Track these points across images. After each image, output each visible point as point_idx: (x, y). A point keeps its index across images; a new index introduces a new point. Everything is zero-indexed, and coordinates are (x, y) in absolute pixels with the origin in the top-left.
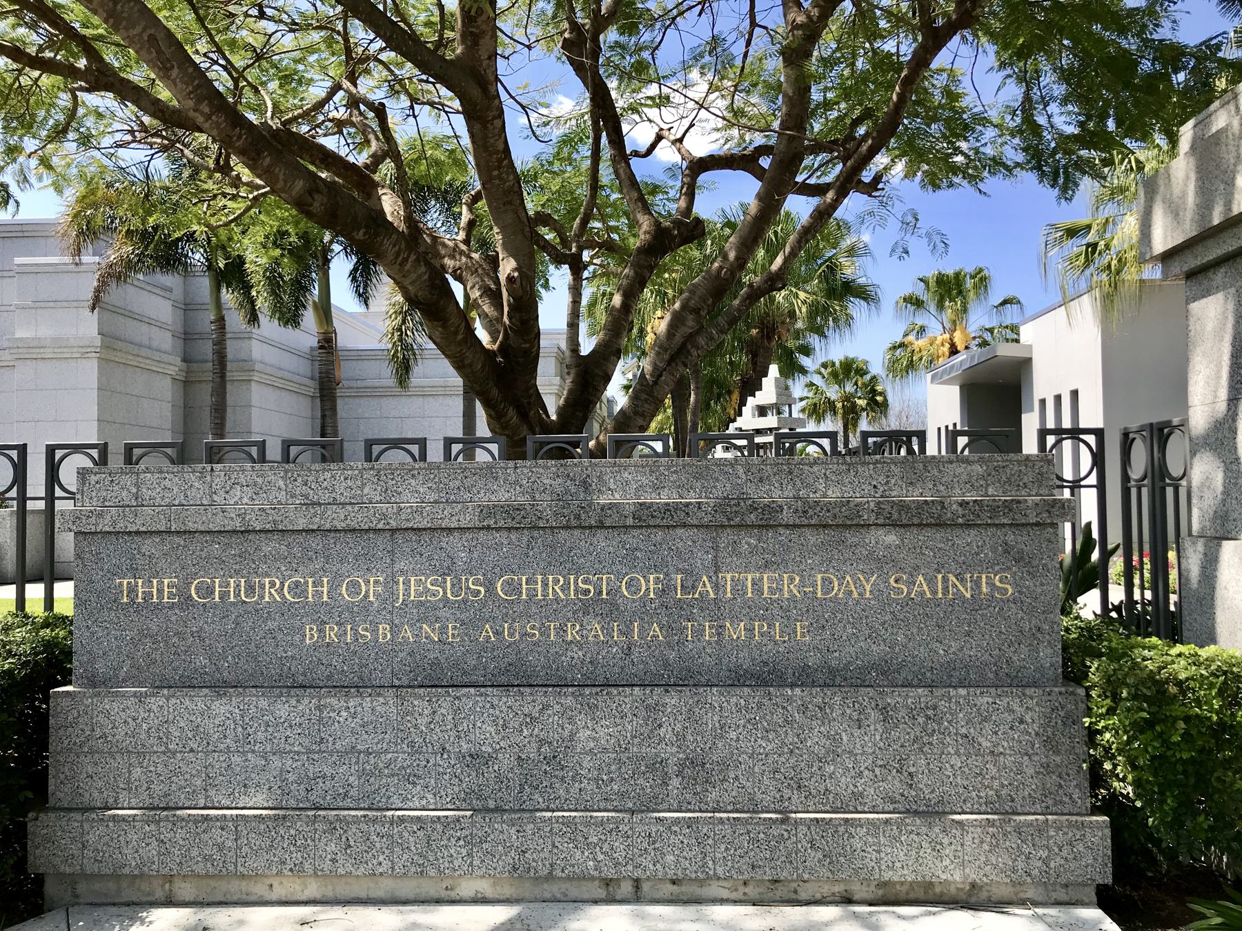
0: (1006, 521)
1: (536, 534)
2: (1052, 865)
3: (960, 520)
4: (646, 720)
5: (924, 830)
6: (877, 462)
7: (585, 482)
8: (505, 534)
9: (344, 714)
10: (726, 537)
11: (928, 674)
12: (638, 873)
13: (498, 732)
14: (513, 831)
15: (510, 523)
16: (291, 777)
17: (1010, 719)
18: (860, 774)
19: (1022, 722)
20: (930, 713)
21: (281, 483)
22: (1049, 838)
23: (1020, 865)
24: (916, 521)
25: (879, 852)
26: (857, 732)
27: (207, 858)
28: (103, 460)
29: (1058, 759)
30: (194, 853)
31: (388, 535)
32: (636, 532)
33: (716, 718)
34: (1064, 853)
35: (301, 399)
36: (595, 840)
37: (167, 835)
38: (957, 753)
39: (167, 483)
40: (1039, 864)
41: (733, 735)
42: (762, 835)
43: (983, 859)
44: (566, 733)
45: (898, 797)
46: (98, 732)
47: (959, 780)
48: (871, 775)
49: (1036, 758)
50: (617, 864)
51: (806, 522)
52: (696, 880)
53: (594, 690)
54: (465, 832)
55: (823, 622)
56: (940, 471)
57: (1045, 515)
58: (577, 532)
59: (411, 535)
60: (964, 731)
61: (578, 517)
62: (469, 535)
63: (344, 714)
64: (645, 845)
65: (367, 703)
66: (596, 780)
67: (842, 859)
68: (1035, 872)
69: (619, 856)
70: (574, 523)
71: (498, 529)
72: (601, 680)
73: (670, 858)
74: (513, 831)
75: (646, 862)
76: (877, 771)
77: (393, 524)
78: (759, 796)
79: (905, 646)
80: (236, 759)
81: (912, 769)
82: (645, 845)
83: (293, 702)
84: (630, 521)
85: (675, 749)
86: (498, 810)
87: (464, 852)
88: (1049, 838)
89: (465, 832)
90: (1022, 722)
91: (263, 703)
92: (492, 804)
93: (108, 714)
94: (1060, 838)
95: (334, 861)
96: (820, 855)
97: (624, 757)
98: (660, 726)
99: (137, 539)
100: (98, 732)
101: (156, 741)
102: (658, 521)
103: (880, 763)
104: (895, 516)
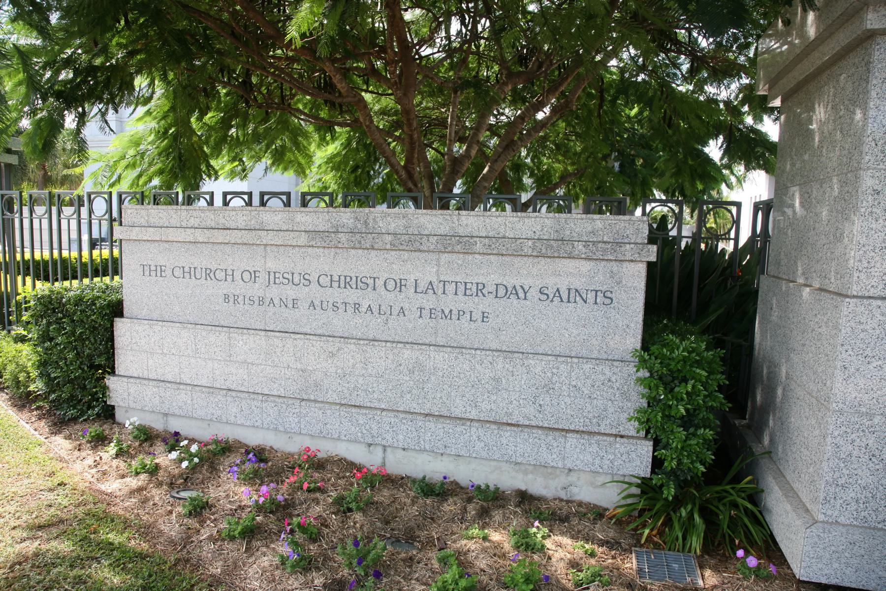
0: (612, 258)
1: (338, 251)
2: (616, 463)
3: (583, 256)
4: (393, 361)
5: (543, 437)
6: (537, 217)
7: (366, 222)
8: (321, 250)
9: (241, 342)
10: (445, 258)
11: (558, 348)
12: (384, 442)
13: (315, 360)
14: (320, 412)
15: (325, 245)
16: (217, 372)
17: (602, 378)
18: (511, 402)
19: (609, 381)
20: (554, 371)
21: (212, 217)
22: (616, 448)
23: (597, 461)
24: (556, 255)
25: (516, 446)
26: (511, 379)
27: (180, 408)
28: (249, 203)
29: (629, 405)
30: (174, 404)
31: (263, 247)
32: (393, 253)
33: (432, 363)
34: (624, 458)
35: (781, 468)
36: (362, 422)
37: (162, 394)
38: (569, 396)
39: (161, 215)
40: (608, 462)
41: (441, 374)
42: (451, 431)
43: (575, 456)
44: (350, 364)
45: (532, 417)
46: (134, 341)
47: (568, 411)
48: (517, 404)
49: (616, 403)
50: (373, 437)
51: (490, 252)
52: (415, 450)
53: (366, 342)
54: (297, 410)
55: (498, 313)
56: (575, 224)
57: (637, 255)
58: (360, 251)
59: (274, 248)
60: (574, 383)
61: (360, 242)
62: (303, 250)
63: (241, 342)
64: (388, 428)
65: (251, 338)
66: (366, 391)
67: (495, 448)
68: (606, 467)
69: (375, 432)
70: (357, 245)
71: (318, 247)
72: (371, 337)
73: (401, 437)
74: (320, 412)
75: (388, 437)
76: (521, 402)
77: (265, 242)
78: (453, 409)
79: (545, 331)
80: (193, 360)
81: (542, 403)
82: (388, 428)
83: (217, 334)
84: (388, 246)
85: (408, 378)
86: (315, 401)
87: (296, 420)
88: (616, 448)
89: (297, 410)
90: (609, 381)
91: (204, 334)
92: (312, 398)
93: (137, 332)
94: (622, 450)
95: (236, 417)
96: (483, 444)
97: (381, 380)
98: (400, 365)
99: (148, 244)
100: (134, 341)
101: (157, 347)
102: (404, 247)
103: (523, 397)
104: (544, 251)
